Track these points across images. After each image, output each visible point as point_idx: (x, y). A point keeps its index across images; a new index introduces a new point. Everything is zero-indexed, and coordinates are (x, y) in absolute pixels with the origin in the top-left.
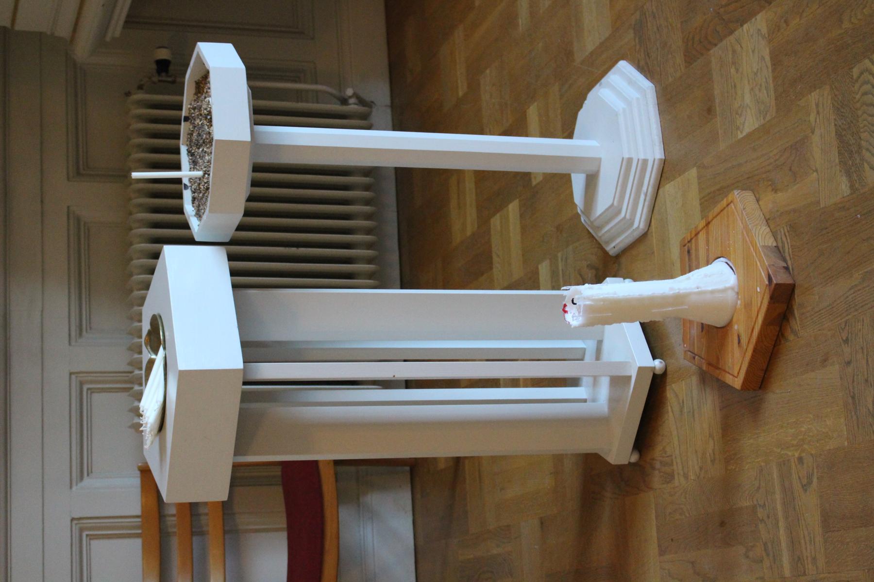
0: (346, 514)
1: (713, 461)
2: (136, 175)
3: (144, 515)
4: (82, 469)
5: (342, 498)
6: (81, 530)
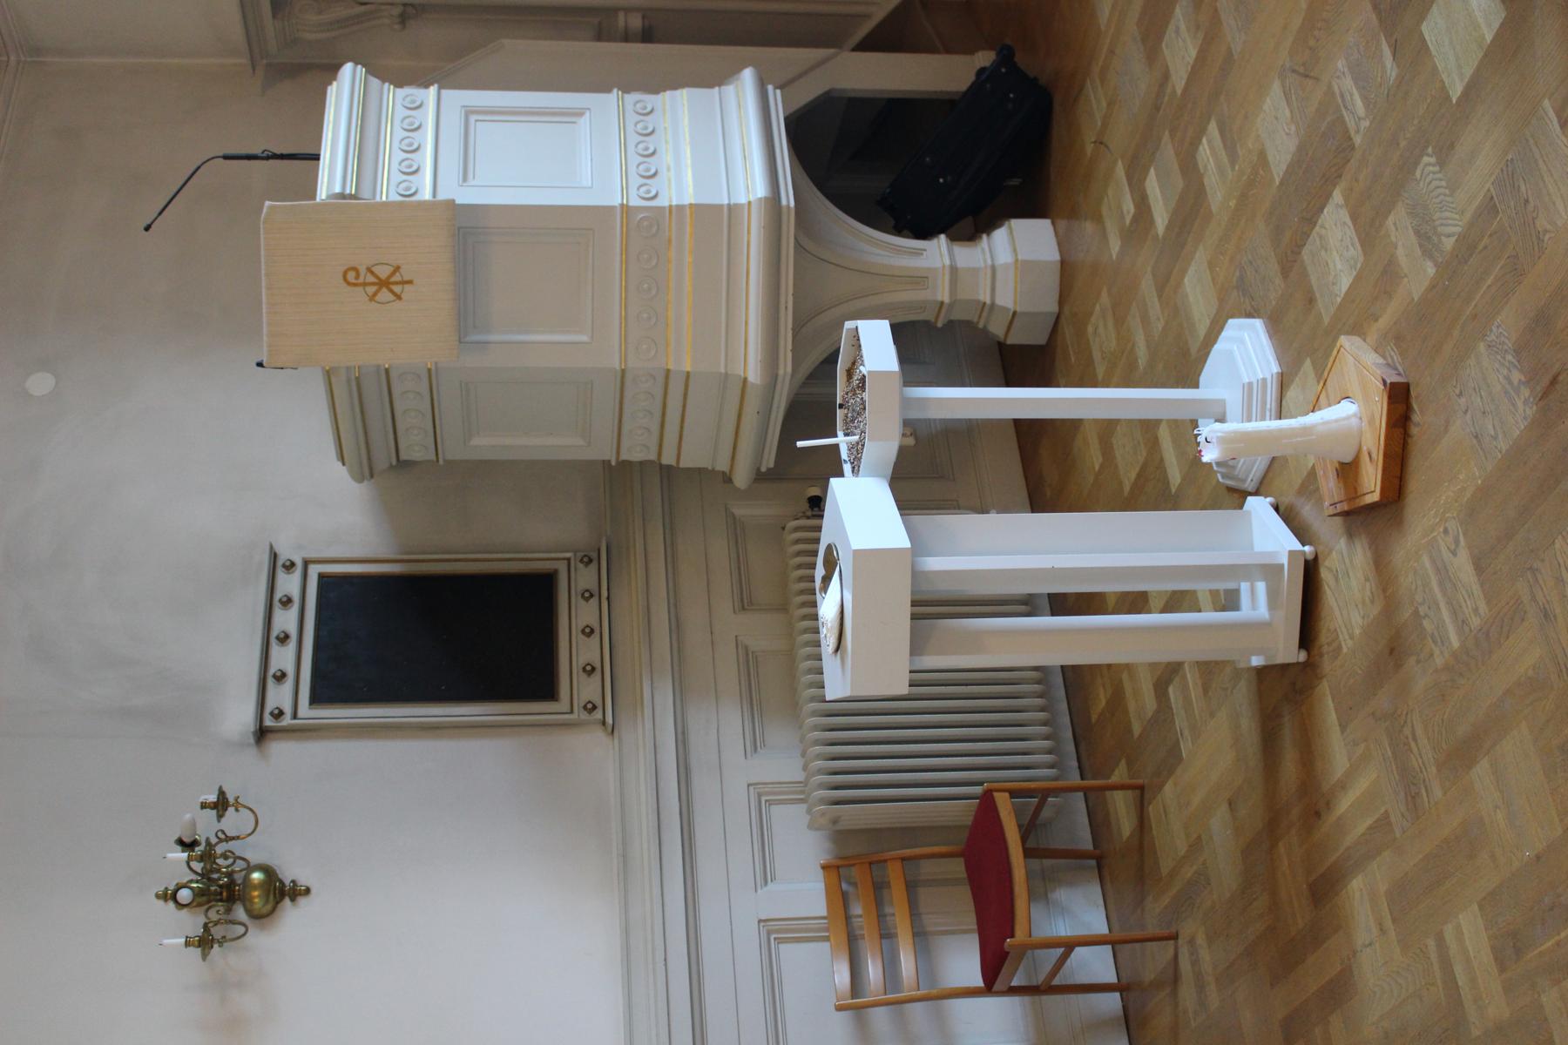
0: (1037, 912)
1: (1372, 602)
2: (800, 444)
3: (830, 916)
4: (766, 875)
5: (1032, 896)
6: (769, 933)
